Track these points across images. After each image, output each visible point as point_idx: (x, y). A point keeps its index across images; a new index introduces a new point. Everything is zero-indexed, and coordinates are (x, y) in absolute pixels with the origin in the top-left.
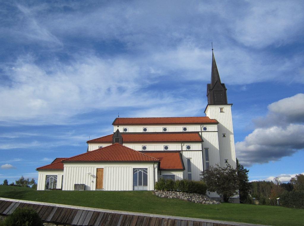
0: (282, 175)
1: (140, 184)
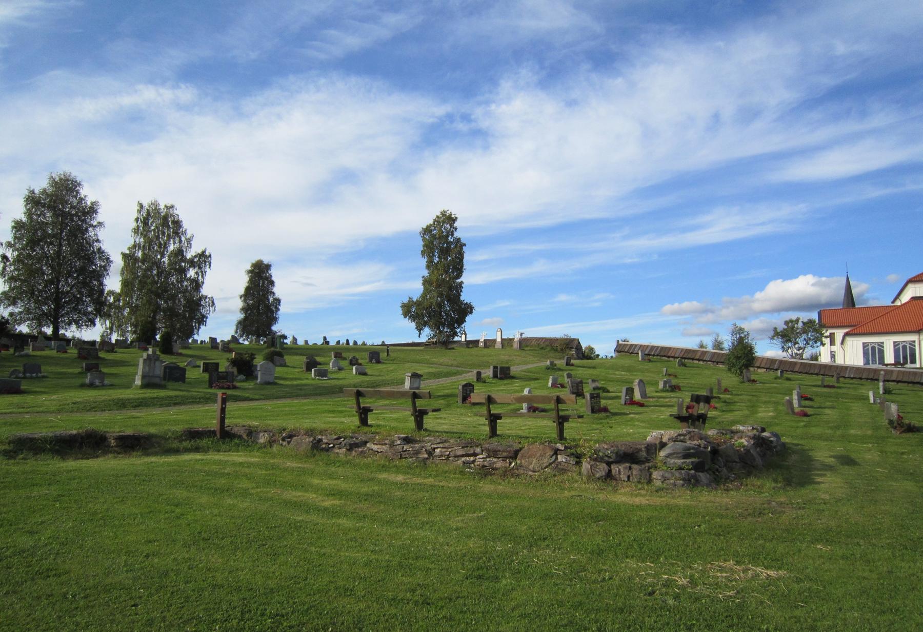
1: (874, 361)
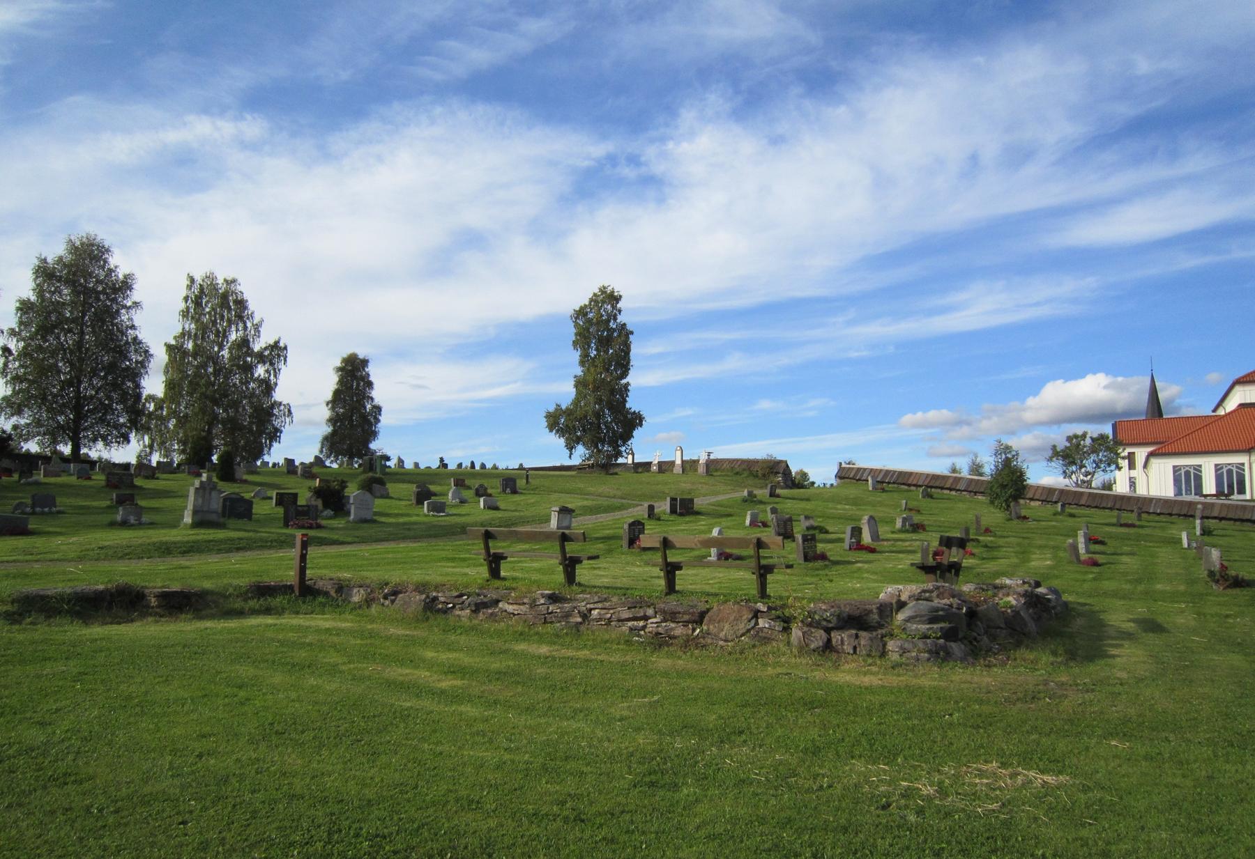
0: (1126, 549)
1: (1188, 491)
